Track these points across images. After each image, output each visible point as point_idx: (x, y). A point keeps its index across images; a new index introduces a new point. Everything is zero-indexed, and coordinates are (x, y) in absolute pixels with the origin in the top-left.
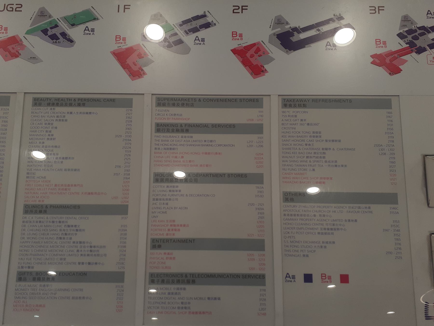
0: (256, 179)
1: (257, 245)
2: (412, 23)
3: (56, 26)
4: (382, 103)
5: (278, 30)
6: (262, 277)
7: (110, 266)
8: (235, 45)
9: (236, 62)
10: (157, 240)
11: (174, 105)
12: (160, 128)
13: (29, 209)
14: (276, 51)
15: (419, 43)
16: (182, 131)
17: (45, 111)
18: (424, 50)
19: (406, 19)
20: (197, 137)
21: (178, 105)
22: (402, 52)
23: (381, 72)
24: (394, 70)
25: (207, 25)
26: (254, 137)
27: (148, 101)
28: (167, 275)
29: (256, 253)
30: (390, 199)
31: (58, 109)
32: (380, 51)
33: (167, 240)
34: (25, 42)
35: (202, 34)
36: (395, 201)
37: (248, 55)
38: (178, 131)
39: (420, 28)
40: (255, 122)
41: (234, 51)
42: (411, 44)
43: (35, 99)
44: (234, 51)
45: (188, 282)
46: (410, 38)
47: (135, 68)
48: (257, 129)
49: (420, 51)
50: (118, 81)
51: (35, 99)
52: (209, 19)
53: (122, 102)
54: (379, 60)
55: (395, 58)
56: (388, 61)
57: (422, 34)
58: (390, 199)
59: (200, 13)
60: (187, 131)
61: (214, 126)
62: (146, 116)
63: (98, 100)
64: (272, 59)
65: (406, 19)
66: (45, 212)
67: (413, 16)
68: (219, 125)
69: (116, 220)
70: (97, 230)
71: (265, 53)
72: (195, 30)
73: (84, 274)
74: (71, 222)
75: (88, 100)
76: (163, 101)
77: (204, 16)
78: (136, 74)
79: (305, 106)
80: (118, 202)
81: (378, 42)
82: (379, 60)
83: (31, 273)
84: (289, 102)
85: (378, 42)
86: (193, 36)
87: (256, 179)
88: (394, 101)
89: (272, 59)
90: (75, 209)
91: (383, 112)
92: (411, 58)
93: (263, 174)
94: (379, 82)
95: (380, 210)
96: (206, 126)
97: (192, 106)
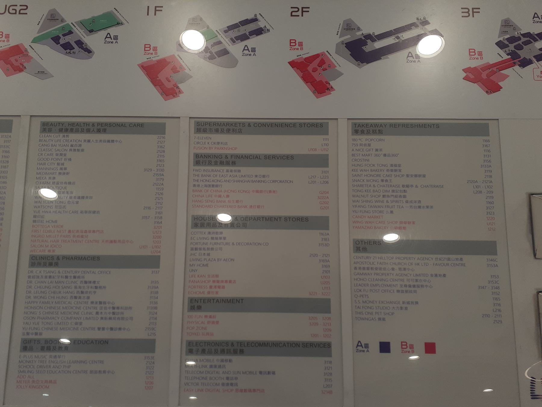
0: (320, 223)
1: (321, 306)
2: (515, 28)
3: (70, 32)
4: (477, 128)
5: (348, 38)
6: (328, 345)
7: (137, 332)
8: (294, 56)
9: (294, 78)
10: (196, 300)
11: (217, 131)
12: (200, 160)
13: (37, 261)
14: (344, 64)
15: (523, 54)
16: (228, 164)
17: (56, 138)
18: (530, 62)
19: (507, 24)
20: (246, 170)
21: (222, 132)
22: (503, 65)
23: (476, 89)
24: (492, 87)
25: (259, 32)
26: (317, 171)
27: (185, 126)
28: (208, 343)
29: (320, 316)
30: (487, 248)
31: (73, 136)
32: (474, 64)
33: (209, 300)
34: (31, 53)
35: (252, 42)
36: (493, 252)
37: (310, 69)
38: (222, 163)
39: (524, 35)
40: (319, 152)
41: (293, 64)
42: (514, 55)
43: (44, 124)
44: (293, 64)
45: (235, 352)
46: (512, 47)
47: (169, 85)
48: (321, 161)
49: (525, 63)
50: (147, 101)
51: (44, 124)
52: (261, 24)
53: (152, 127)
54: (473, 75)
55: (494, 73)
56: (484, 76)
57: (527, 43)
58: (487, 248)
59: (250, 16)
60: (234, 163)
61: (268, 157)
62: (182, 145)
63: (122, 125)
64: (340, 74)
65: (507, 24)
66: (57, 265)
67: (516, 20)
68: (274, 157)
69: (145, 275)
70: (121, 288)
71: (331, 66)
72: (243, 38)
73: (105, 342)
74: (89, 277)
75: (110, 125)
76: (204, 126)
77: (255, 20)
78: (170, 92)
79: (380, 132)
80: (148, 252)
81: (472, 52)
82: (473, 75)
83: (39, 341)
84: (360, 128)
85: (472, 52)
86: (241, 45)
87: (320, 223)
88: (492, 126)
89: (340, 74)
90: (94, 261)
91: (479, 140)
92: (513, 73)
94: (474, 103)
95: (474, 262)
96: (257, 157)
97: (240, 132)
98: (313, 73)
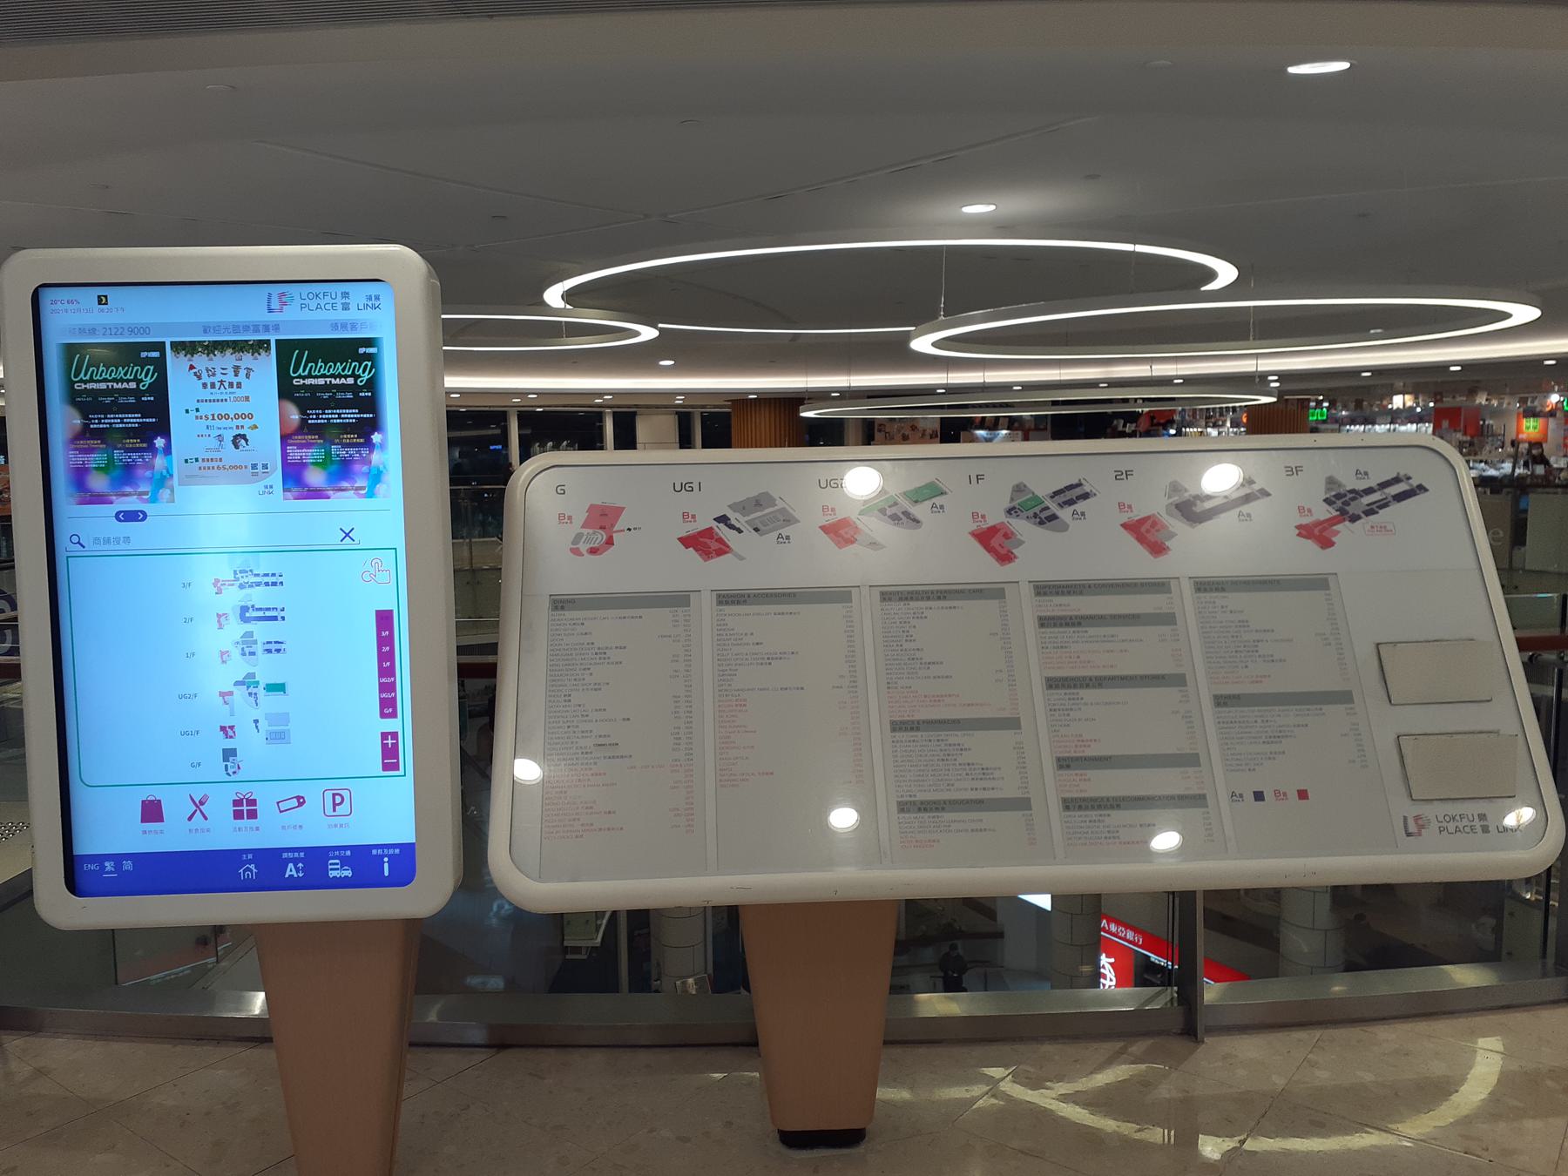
0: (1178, 680)
1: (1191, 760)
2: (1340, 485)
3: (896, 504)
4: (1318, 583)
5: (1176, 499)
6: (1203, 797)
7: (1010, 791)
8: (1124, 518)
9: (1129, 539)
10: (1064, 759)
11: (1057, 594)
12: (1044, 622)
13: (897, 726)
14: (1176, 525)
15: (1351, 509)
16: (1073, 625)
17: (896, 607)
18: (1359, 518)
19: (1331, 482)
20: (1092, 631)
21: (1063, 594)
22: (1333, 521)
23: (1310, 545)
24: (1326, 543)
25: (1086, 496)
26: (1166, 629)
27: (1026, 591)
28: (1084, 799)
29: (1191, 770)
30: (1345, 697)
31: (913, 604)
32: (1306, 521)
33: (1077, 759)
34: (861, 526)
35: (1080, 506)
36: (1351, 701)
37: (1143, 529)
38: (1067, 625)
39: (1351, 491)
40: (1165, 610)
41: (1125, 526)
42: (1343, 512)
43: (882, 593)
44: (1125, 526)
45: (1112, 807)
46: (1339, 503)
47: (1003, 552)
48: (1168, 619)
49: (1354, 519)
50: (1135, 562)
51: (882, 593)
52: (1087, 488)
53: (992, 593)
54: (1305, 531)
55: (1325, 529)
56: (1316, 532)
57: (1353, 499)
58: (1345, 697)
59: (1075, 481)
60: (1079, 624)
61: (1113, 617)
62: (1027, 608)
63: (962, 591)
64: (1021, 543)
65: (1331, 482)
66: (918, 729)
67: (1340, 478)
68: (1120, 616)
69: (1007, 736)
70: (984, 747)
71: (1164, 527)
72: (1070, 502)
73: (981, 801)
74: (952, 740)
75: (950, 592)
76: (1043, 589)
77: (1079, 485)
78: (1157, 549)
79: (1223, 590)
80: (1006, 714)
81: (1301, 509)
82: (1305, 531)
83: (914, 803)
84: (1203, 586)
85: (1301, 509)
86: (1069, 510)
87: (1178, 680)
88: (1008, 589)
89: (1021, 543)
90: (955, 724)
91: (1319, 595)
92: (1344, 528)
93: (378, 612)
94: (1309, 558)
95: (1335, 711)
96: (1102, 617)
97: (1081, 593)
98: (994, 541)
